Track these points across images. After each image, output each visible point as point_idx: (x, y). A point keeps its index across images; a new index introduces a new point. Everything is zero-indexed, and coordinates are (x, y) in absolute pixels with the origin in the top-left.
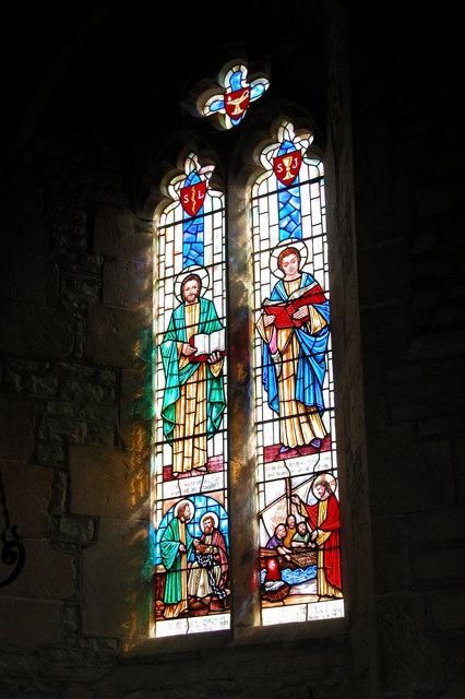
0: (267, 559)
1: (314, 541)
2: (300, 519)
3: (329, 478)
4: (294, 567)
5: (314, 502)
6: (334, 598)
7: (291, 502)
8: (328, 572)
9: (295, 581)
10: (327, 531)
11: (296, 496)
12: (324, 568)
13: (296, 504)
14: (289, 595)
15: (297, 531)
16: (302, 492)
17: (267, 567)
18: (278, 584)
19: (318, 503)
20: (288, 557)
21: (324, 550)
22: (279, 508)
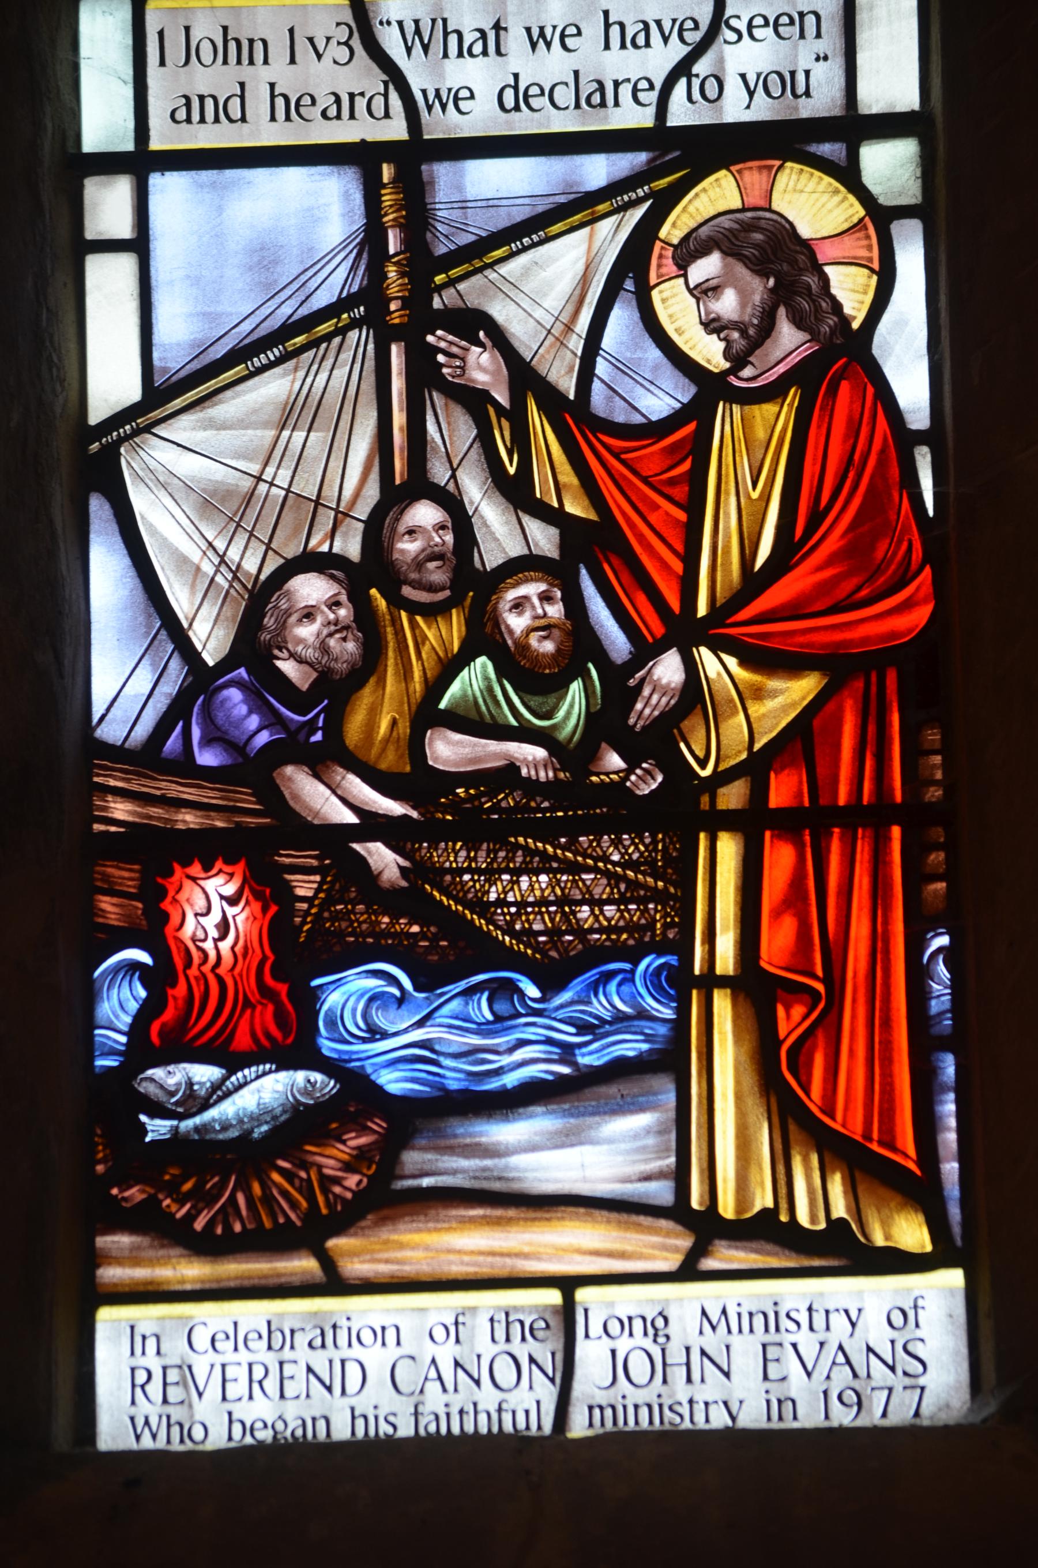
0: (162, 856)
1: (658, 742)
2: (501, 532)
3: (809, 204)
4: (446, 951)
5: (659, 399)
6: (842, 1251)
7: (424, 375)
8: (791, 1021)
9: (454, 1076)
10: (788, 664)
11: (474, 325)
12: (754, 987)
13: (474, 401)
14: (388, 1199)
15: (484, 637)
16: (538, 294)
17: (154, 927)
18: (266, 1091)
19: (697, 415)
20: (383, 858)
21: (753, 825)
22: (288, 416)
